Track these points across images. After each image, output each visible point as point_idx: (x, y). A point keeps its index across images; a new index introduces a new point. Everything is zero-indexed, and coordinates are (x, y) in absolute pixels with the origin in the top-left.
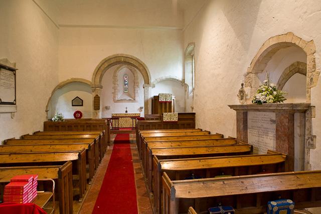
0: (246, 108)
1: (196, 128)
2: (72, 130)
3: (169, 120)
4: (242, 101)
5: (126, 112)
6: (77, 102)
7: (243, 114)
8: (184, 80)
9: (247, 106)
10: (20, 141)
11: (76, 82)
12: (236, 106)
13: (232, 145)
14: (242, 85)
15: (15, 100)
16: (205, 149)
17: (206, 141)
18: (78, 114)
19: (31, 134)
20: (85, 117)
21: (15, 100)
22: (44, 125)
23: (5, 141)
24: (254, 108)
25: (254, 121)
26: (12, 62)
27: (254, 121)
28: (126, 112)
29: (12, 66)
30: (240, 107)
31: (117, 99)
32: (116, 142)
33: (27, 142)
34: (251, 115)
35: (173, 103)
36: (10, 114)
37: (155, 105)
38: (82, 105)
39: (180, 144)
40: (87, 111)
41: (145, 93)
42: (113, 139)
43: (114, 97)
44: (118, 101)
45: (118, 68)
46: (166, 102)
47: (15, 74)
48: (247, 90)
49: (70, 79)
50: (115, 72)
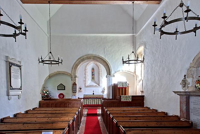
0: (189, 94)
1: (145, 107)
2: (60, 107)
3: (125, 100)
4: (184, 88)
5: (93, 94)
6: (62, 87)
7: (186, 97)
8: (135, 72)
9: (189, 92)
10: (25, 114)
11: (60, 73)
12: (180, 92)
13: (176, 121)
14: (185, 76)
15: (21, 87)
16: (155, 122)
17: (156, 117)
18: (61, 95)
19: (23, 112)
20: (66, 97)
21: (21, 87)
22: (40, 103)
23: (15, 115)
24: (196, 94)
25: (195, 103)
26: (18, 59)
27: (195, 103)
28: (93, 94)
29: (18, 64)
30: (183, 93)
31: (87, 85)
32: (88, 115)
33: (29, 116)
34: (192, 99)
35: (127, 88)
36: (134, 64)
37: (115, 92)
38: (65, 90)
39: (137, 119)
40: (68, 94)
41: (109, 81)
42: (86, 113)
43: (85, 84)
44: (88, 86)
45: (88, 64)
46: (122, 88)
47: (21, 69)
48: (189, 80)
49: (56, 71)
50: (86, 67)
